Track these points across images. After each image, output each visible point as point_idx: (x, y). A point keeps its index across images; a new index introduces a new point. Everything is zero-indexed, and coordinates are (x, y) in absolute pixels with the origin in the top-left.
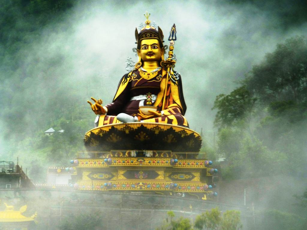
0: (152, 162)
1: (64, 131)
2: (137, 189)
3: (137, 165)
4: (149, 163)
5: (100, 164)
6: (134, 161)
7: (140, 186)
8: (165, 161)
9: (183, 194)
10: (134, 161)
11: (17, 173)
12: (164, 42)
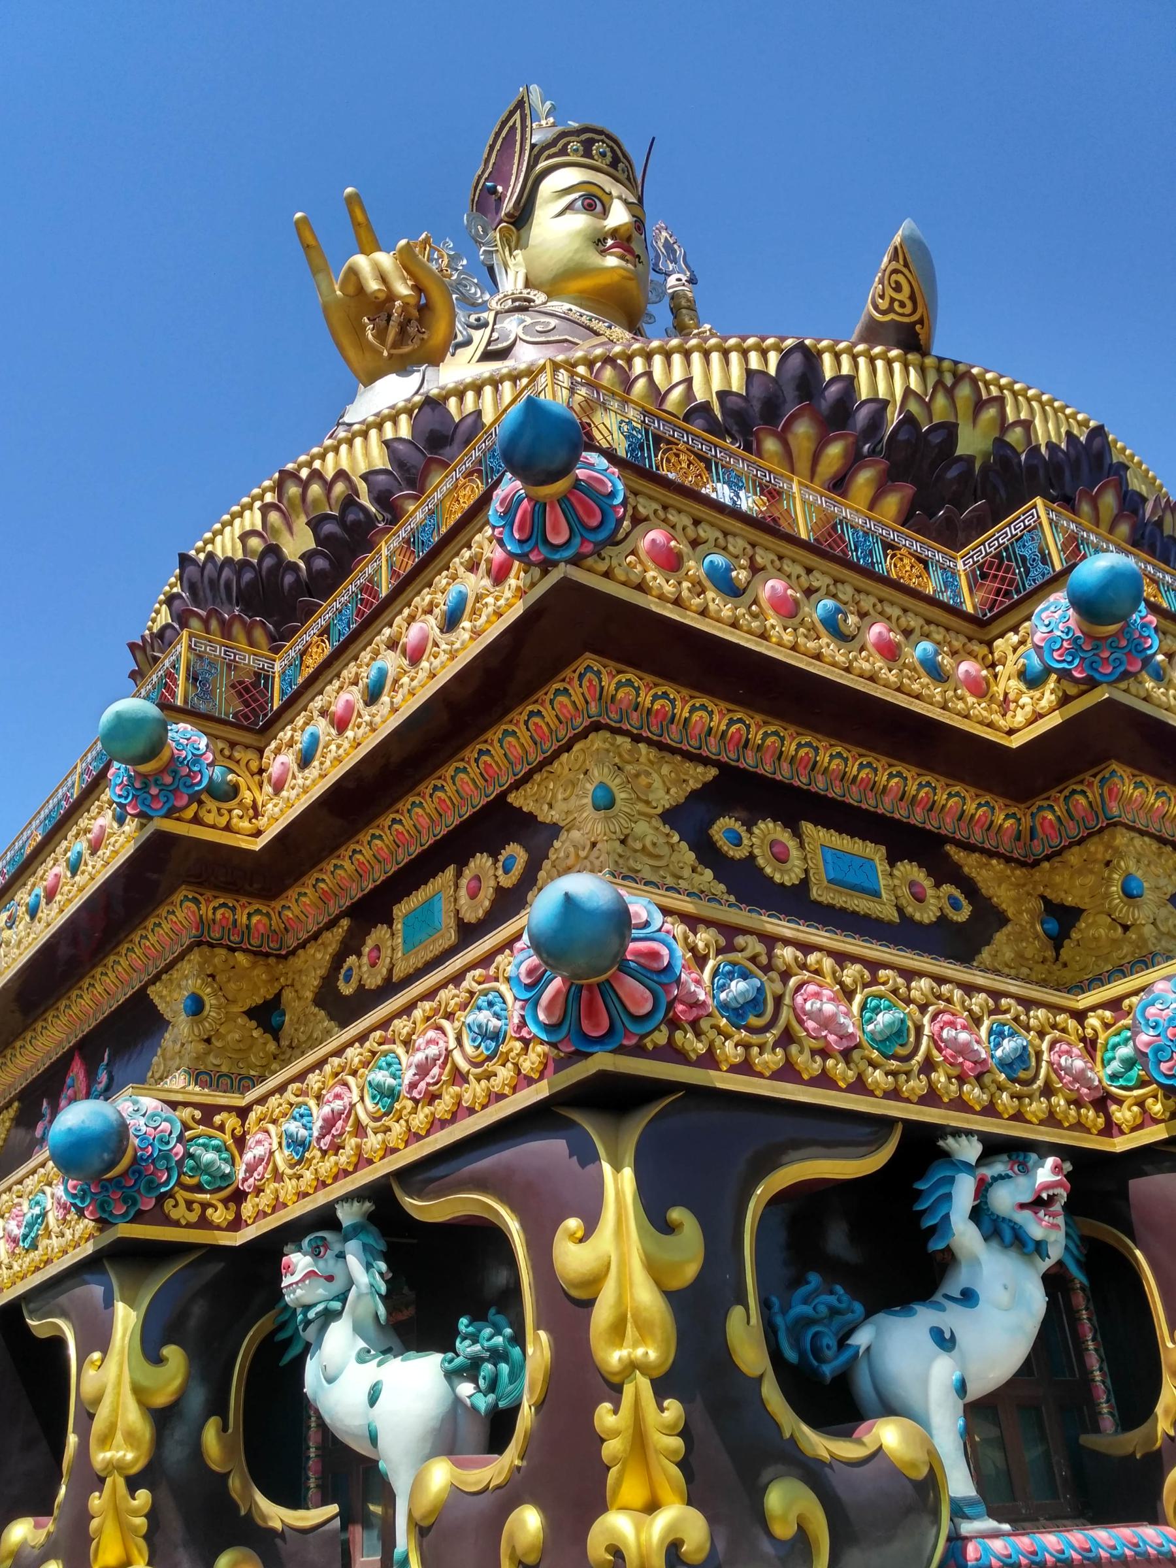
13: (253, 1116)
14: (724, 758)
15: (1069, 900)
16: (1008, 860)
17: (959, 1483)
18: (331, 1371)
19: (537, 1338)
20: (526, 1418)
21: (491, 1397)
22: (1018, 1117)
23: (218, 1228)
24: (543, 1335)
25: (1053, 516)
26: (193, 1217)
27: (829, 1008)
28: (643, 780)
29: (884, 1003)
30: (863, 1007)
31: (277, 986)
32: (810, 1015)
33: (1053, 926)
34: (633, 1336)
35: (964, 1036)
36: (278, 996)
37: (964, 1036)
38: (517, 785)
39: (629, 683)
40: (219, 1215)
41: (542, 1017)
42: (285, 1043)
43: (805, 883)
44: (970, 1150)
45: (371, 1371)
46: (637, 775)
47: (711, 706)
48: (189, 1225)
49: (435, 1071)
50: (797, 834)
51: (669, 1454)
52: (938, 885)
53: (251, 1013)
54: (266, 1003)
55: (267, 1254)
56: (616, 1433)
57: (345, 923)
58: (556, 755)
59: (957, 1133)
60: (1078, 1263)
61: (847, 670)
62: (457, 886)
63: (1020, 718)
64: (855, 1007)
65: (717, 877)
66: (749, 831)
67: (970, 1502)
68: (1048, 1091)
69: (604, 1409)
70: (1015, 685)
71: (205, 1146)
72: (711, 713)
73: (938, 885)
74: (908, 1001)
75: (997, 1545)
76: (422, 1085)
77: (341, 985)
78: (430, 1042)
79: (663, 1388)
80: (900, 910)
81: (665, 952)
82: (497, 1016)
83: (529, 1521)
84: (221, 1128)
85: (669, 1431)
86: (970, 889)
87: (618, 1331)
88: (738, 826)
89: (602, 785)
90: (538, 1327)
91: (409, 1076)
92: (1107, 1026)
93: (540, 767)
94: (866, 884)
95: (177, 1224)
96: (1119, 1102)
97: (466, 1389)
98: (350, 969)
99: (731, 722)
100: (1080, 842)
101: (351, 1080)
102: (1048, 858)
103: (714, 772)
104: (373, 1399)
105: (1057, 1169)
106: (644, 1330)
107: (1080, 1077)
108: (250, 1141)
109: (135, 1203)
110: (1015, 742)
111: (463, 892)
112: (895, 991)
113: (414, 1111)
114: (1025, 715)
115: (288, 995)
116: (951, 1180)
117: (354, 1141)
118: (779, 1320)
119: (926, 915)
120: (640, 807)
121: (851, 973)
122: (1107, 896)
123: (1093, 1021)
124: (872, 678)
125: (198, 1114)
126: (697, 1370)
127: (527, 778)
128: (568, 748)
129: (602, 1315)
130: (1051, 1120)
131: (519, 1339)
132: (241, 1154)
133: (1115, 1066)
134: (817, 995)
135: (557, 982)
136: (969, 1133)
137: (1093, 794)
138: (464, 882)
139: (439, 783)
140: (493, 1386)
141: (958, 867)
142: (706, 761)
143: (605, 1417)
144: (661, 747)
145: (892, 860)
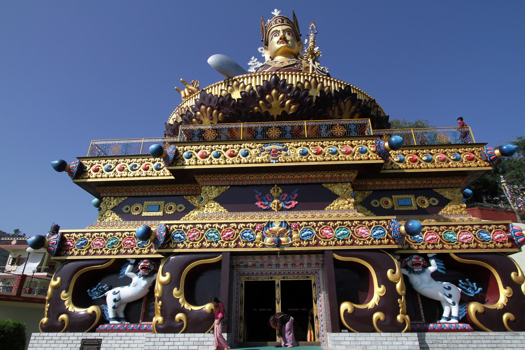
0: (312, 151)
1: (238, 99)
2: (264, 246)
3: (262, 162)
4: (304, 154)
5: (146, 169)
6: (253, 152)
7: (273, 233)
8: (357, 148)
9: (433, 262)
10: (253, 152)
11: (147, 141)
12: (301, 35)
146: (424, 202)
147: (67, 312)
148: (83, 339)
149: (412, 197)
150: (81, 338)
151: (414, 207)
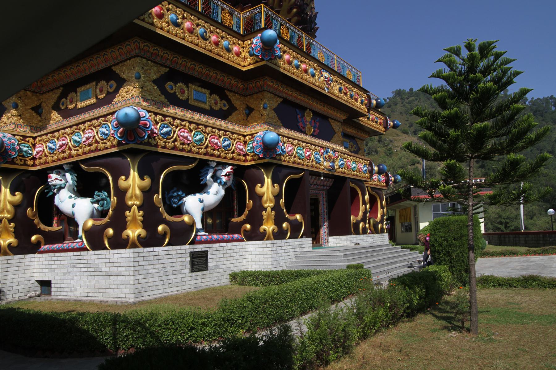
12: (411, 90)
13: (37, 140)
14: (171, 66)
15: (252, 106)
16: (240, 95)
17: (199, 225)
18: (62, 200)
19: (114, 199)
20: (111, 212)
21: (102, 208)
22: (225, 158)
23: (29, 166)
24: (115, 198)
25: (265, 9)
26: (22, 163)
27: (186, 134)
28: (149, 71)
29: (199, 133)
30: (194, 134)
31: (40, 102)
32: (181, 136)
33: (247, 112)
34: (134, 200)
35: (216, 141)
36: (40, 104)
37: (216, 141)
38: (114, 65)
39: (147, 46)
40: (30, 163)
41: (119, 135)
42: (43, 118)
43: (188, 100)
44: (214, 164)
45: (72, 201)
46: (147, 70)
47: (169, 53)
48: (21, 165)
49: (91, 139)
50: (188, 87)
51: (140, 220)
52: (221, 101)
53: (33, 109)
54: (37, 106)
55: (43, 175)
56: (129, 216)
57: (62, 88)
58: (126, 60)
59: (211, 161)
60: (234, 186)
61: (205, 49)
62: (96, 88)
63: (246, 64)
64: (192, 134)
65: (166, 98)
66: (176, 86)
67: (200, 229)
68: (233, 152)
69: (127, 213)
70: (247, 54)
71: (24, 146)
72: (169, 55)
73: (221, 101)
74: (205, 133)
75: (204, 237)
76: (87, 142)
77: (61, 106)
78: (89, 133)
79: (140, 208)
80: (211, 107)
81: (148, 123)
82: (107, 130)
83: (111, 231)
84: (28, 142)
85: (140, 216)
86: (229, 101)
87: (131, 198)
88: (172, 84)
89: (138, 73)
90: (114, 196)
91: (84, 139)
92: (250, 139)
93: (121, 62)
94: (203, 100)
95: (17, 164)
96: (248, 155)
97: (96, 205)
98: (63, 102)
99: (174, 57)
100: (257, 93)
101: (67, 136)
102: (249, 95)
103: (168, 70)
104: (73, 206)
105: (231, 169)
106: (137, 198)
107: (242, 150)
108: (37, 146)
109: (6, 159)
110: (244, 69)
111: (98, 90)
112: (202, 131)
113: (85, 147)
114: (246, 64)
115: (44, 105)
116: (208, 170)
117: (68, 151)
118: (166, 196)
119: (217, 108)
120: (147, 78)
121: (192, 126)
122: (260, 107)
123: (247, 138)
124: (211, 51)
125: (22, 138)
126: (147, 205)
127: (118, 64)
128: (130, 59)
129: (129, 194)
130: (232, 159)
131: (109, 196)
132: (34, 149)
133: (249, 148)
134: (184, 132)
135: (121, 129)
136: (214, 161)
137: (261, 83)
138: (98, 87)
139: (92, 59)
140: (102, 205)
141: (227, 96)
142: (166, 67)
143: (127, 213)
144: (155, 62)
145: (211, 94)
146: (216, 103)
147: (165, 222)
148: (191, 252)
149: (207, 92)
150: (189, 251)
151: (207, 107)
